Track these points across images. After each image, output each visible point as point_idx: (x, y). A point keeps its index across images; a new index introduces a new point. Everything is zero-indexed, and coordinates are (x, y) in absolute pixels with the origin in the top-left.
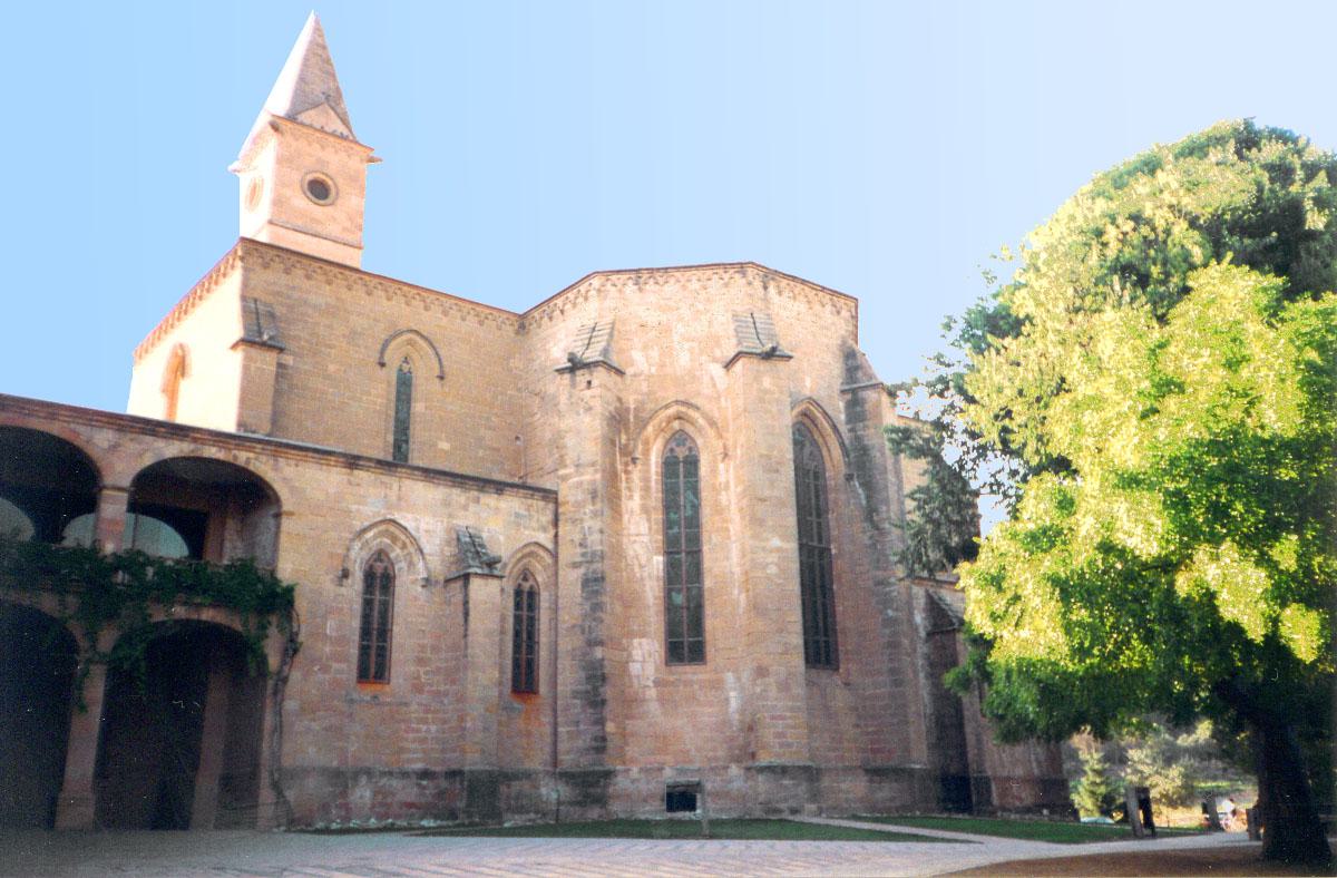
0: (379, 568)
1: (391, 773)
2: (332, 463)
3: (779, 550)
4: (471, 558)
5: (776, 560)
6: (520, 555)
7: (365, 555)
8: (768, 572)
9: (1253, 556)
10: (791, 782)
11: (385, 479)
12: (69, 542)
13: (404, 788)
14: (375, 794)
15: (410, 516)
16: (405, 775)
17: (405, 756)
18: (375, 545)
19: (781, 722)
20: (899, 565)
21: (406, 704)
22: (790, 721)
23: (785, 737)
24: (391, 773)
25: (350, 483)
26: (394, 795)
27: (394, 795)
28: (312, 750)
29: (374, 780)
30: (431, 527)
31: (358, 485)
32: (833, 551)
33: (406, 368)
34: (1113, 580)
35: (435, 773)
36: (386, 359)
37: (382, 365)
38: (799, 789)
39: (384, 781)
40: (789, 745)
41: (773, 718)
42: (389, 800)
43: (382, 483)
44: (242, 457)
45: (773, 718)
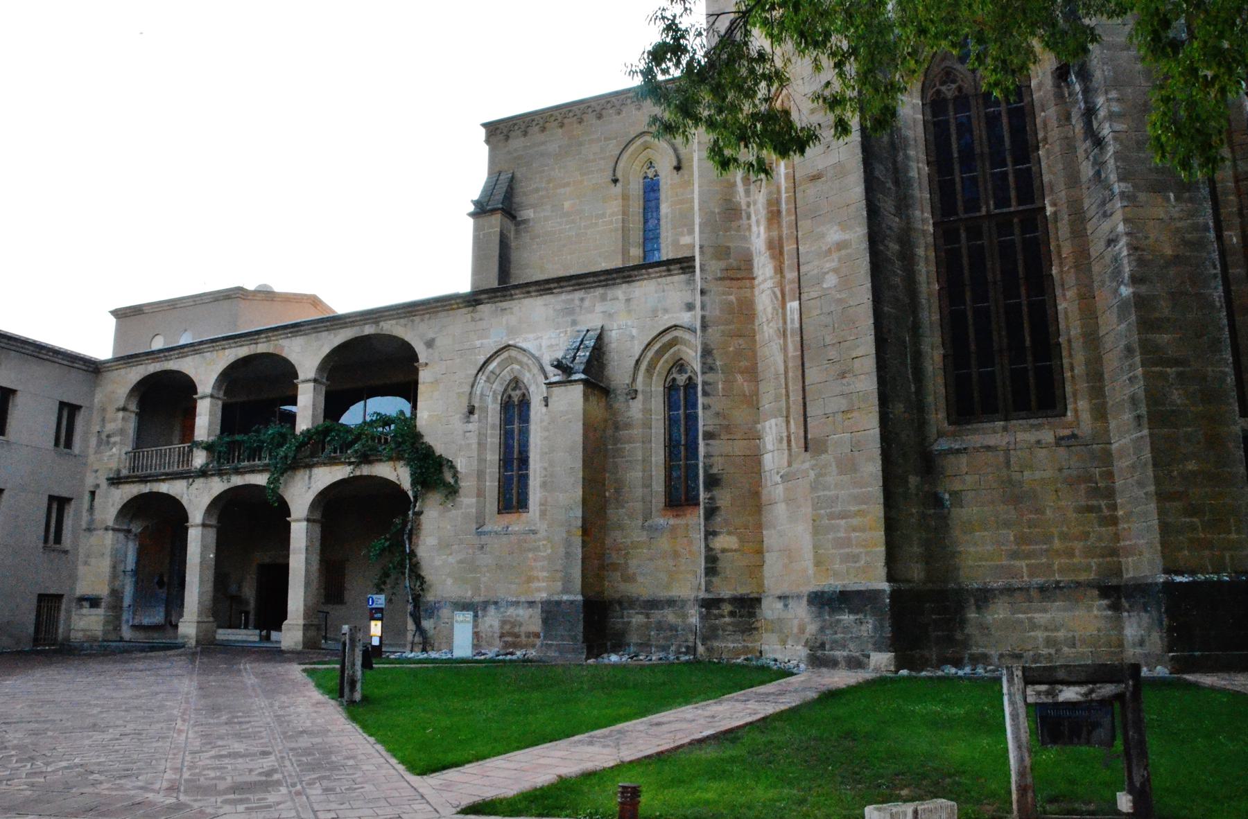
0: (516, 395)
1: (516, 604)
2: (455, 306)
3: (841, 246)
4: (254, 460)
5: (834, 264)
6: (657, 346)
7: (498, 387)
8: (825, 286)
9: (274, 502)
10: (852, 617)
11: (504, 305)
12: (340, 422)
13: (531, 617)
14: (504, 623)
15: (531, 336)
16: (531, 604)
17: (535, 585)
18: (506, 375)
19: (843, 522)
20: (110, 532)
21: (534, 532)
22: (856, 521)
23: (849, 545)
24: (516, 604)
25: (473, 320)
26: (521, 625)
27: (521, 625)
28: (449, 581)
29: (502, 610)
30: (554, 342)
31: (481, 319)
32: (1049, 210)
33: (650, 174)
34: (836, 18)
35: (992, 590)
36: (619, 175)
37: (615, 181)
38: (863, 628)
39: (511, 611)
40: (855, 558)
41: (831, 516)
42: (516, 630)
43: (502, 310)
44: (172, 365)
45: (831, 516)
